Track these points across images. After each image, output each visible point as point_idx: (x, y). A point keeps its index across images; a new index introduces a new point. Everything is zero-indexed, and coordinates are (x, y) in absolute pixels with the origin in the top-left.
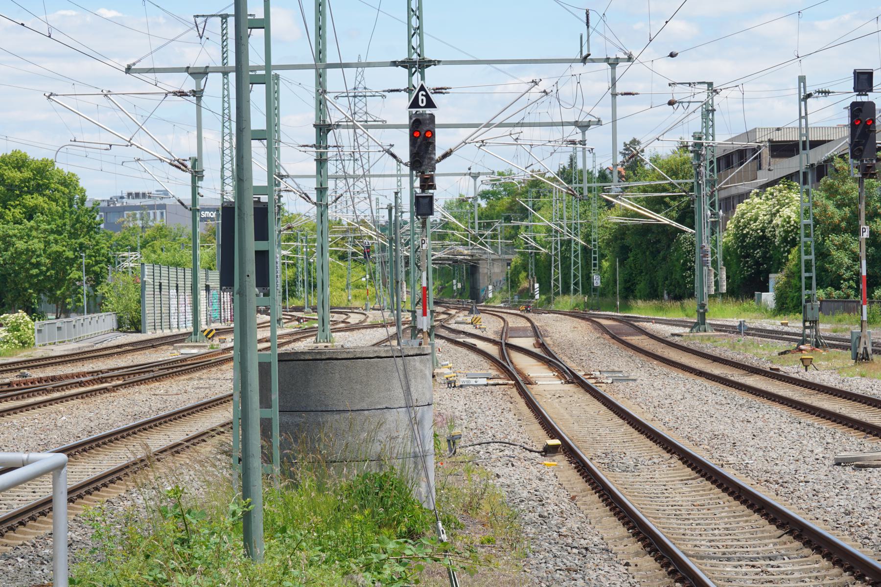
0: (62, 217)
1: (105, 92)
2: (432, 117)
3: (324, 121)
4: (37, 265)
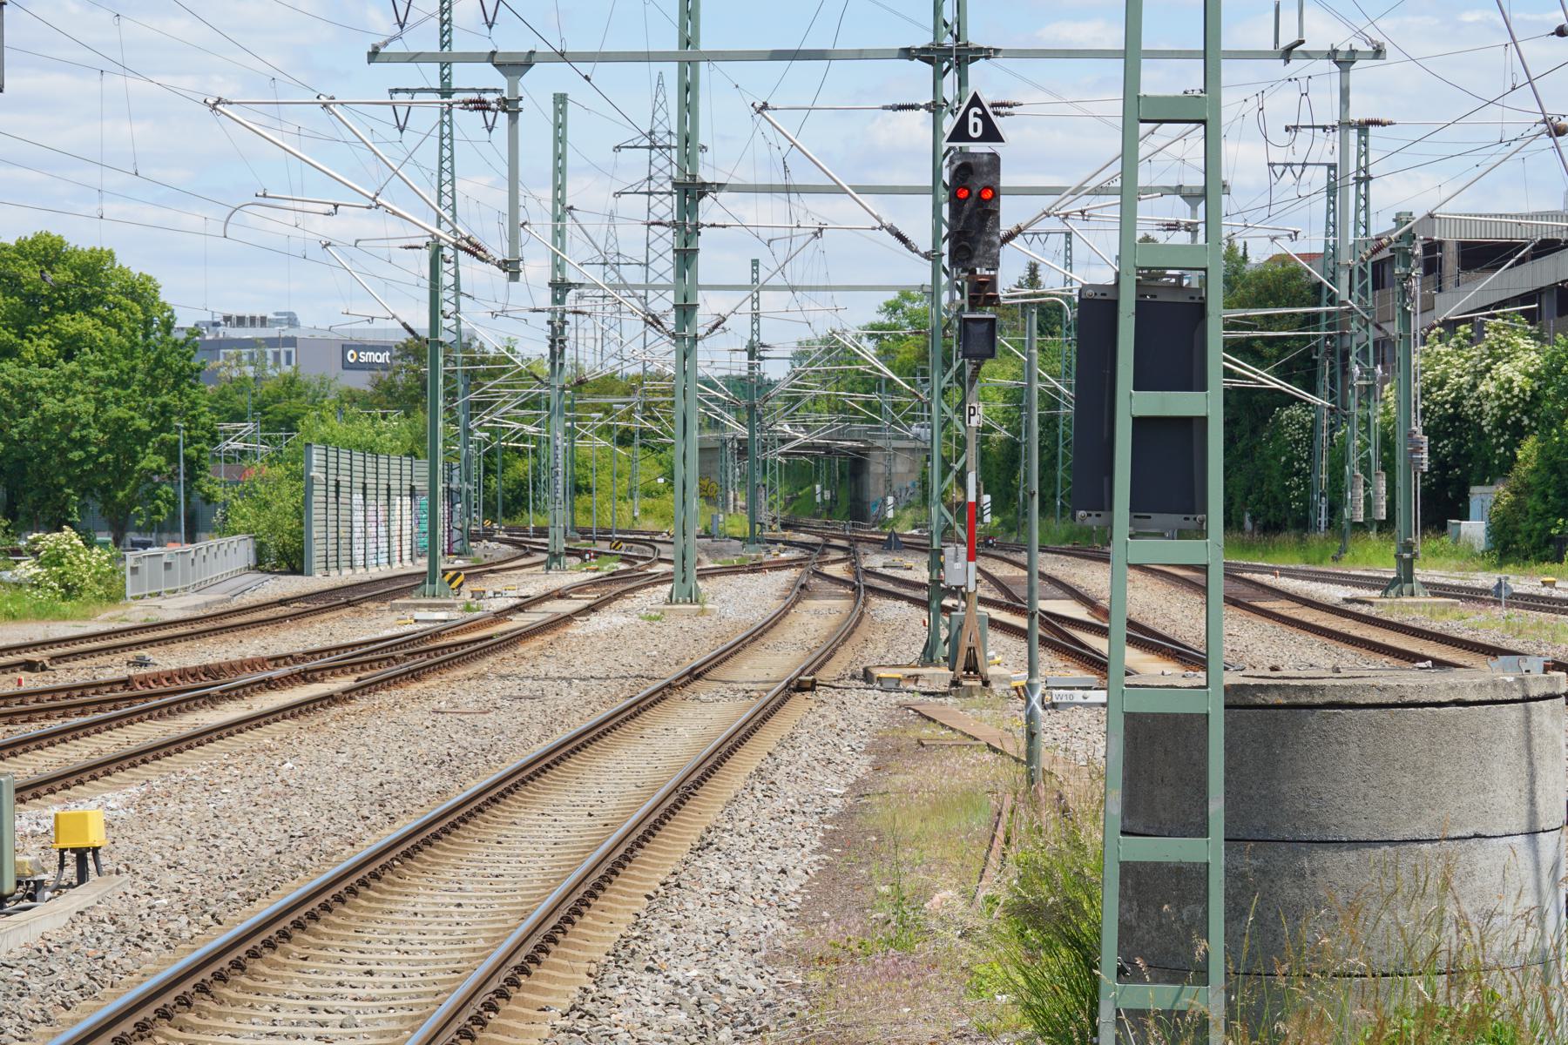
0: (129, 354)
1: (323, 99)
2: (995, 159)
3: (694, 176)
4: (82, 443)
